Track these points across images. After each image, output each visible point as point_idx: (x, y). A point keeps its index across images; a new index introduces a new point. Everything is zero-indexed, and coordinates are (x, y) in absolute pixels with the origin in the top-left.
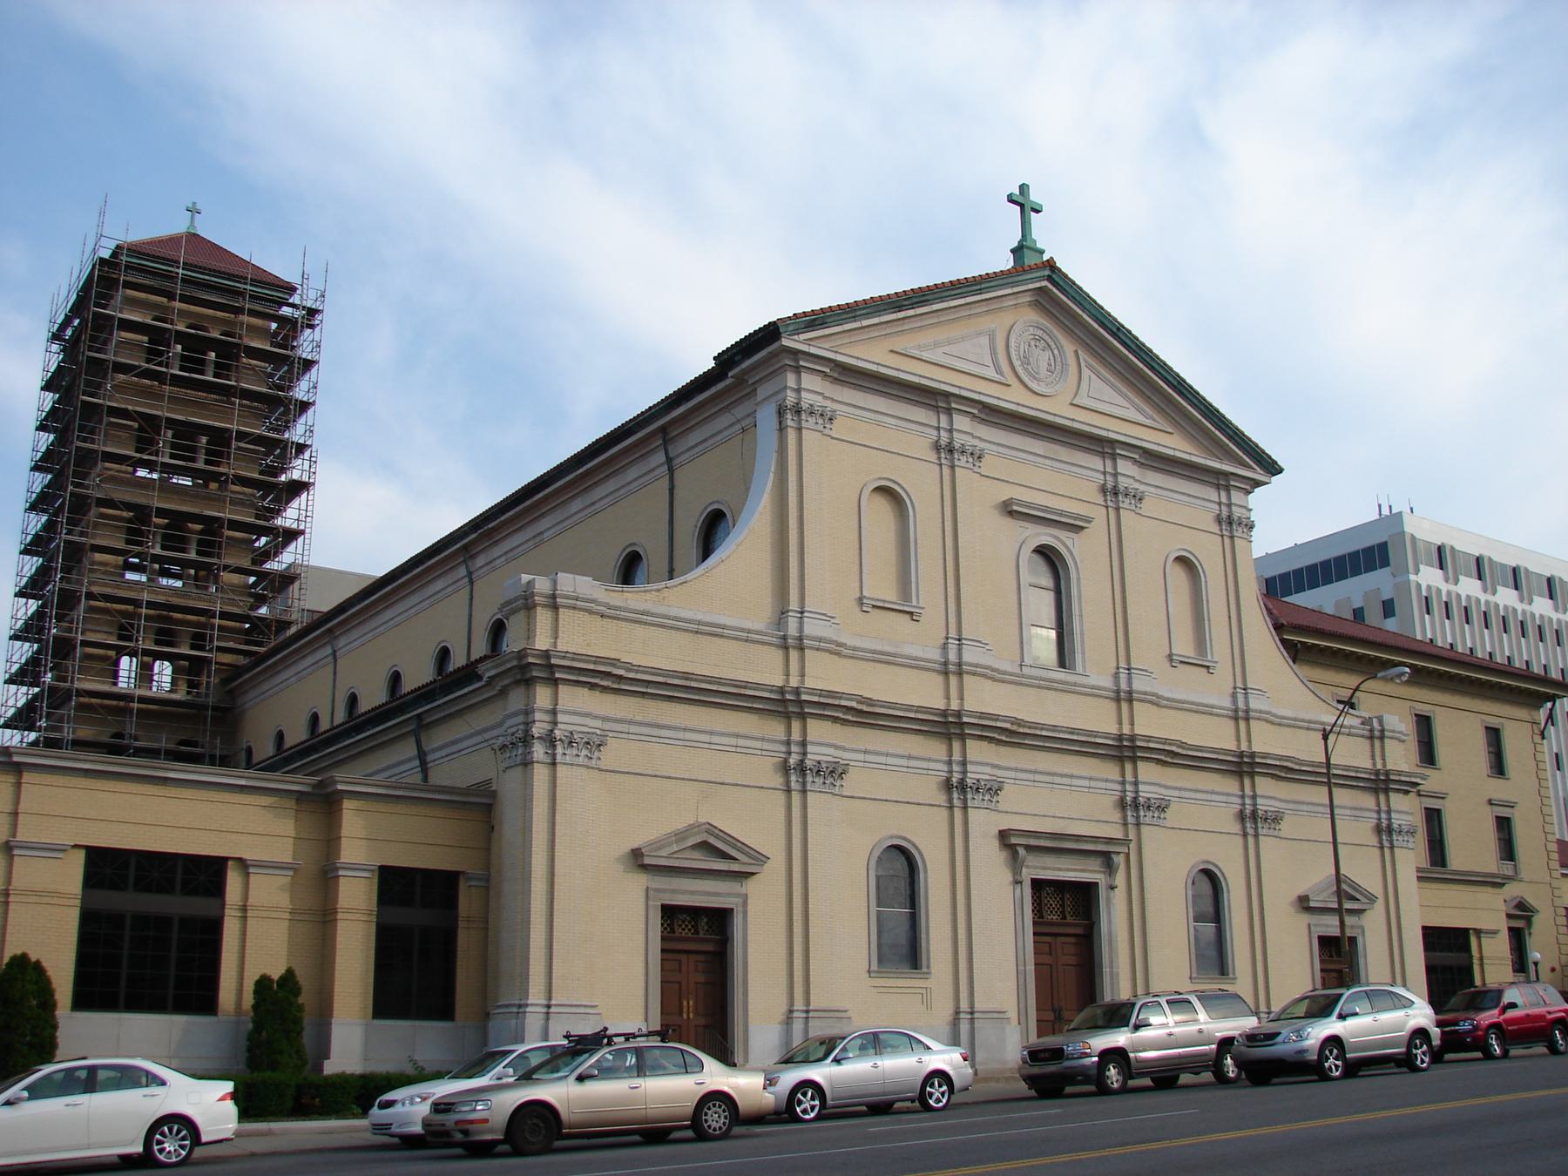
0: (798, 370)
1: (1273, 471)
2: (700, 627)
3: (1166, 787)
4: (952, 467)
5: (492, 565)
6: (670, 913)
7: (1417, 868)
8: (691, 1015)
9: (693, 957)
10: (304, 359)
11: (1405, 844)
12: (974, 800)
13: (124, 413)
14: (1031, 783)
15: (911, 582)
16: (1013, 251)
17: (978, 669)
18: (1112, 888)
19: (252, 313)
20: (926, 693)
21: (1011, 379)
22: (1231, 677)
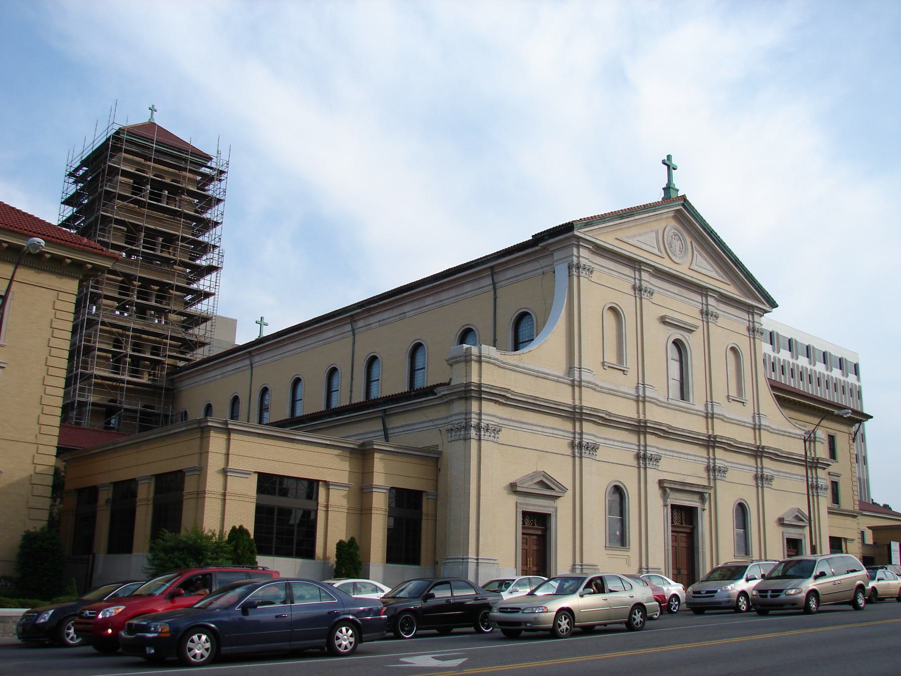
4: (641, 298)
5: (370, 326)
6: (525, 514)
7: (828, 507)
10: (217, 199)
11: (823, 494)
12: (650, 464)
14: (671, 457)
16: (664, 189)
18: (704, 510)
20: (627, 410)
21: (665, 255)
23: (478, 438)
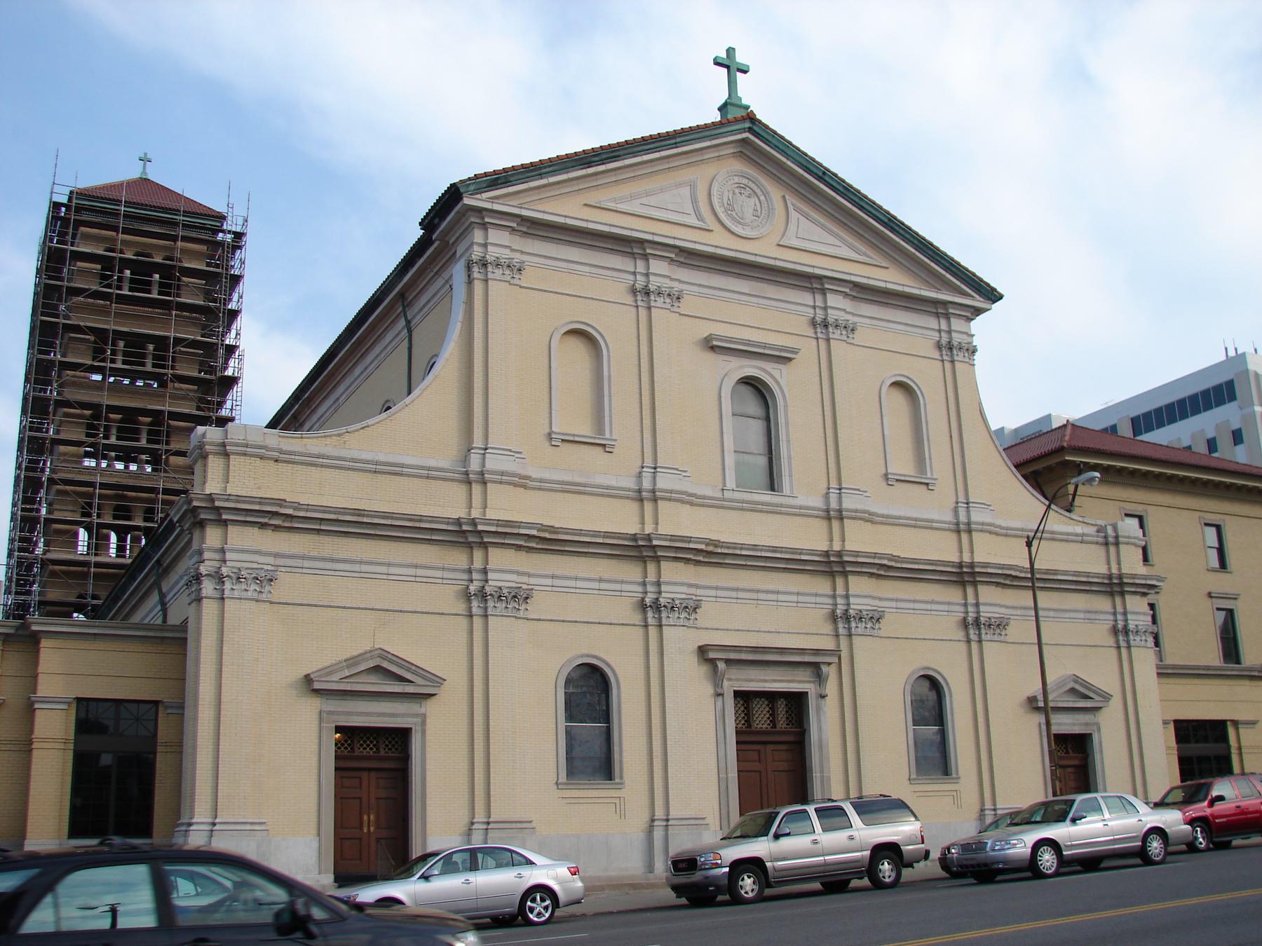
0: (484, 226)
1: (993, 298)
2: (378, 467)
3: (880, 599)
8: (372, 829)
9: (373, 774)
13: (77, 329)
15: (925, 459)
17: (673, 495)
18: (823, 697)
19: (185, 239)
20: (943, 549)
21: (711, 223)
22: (953, 492)
23: (1115, 645)
